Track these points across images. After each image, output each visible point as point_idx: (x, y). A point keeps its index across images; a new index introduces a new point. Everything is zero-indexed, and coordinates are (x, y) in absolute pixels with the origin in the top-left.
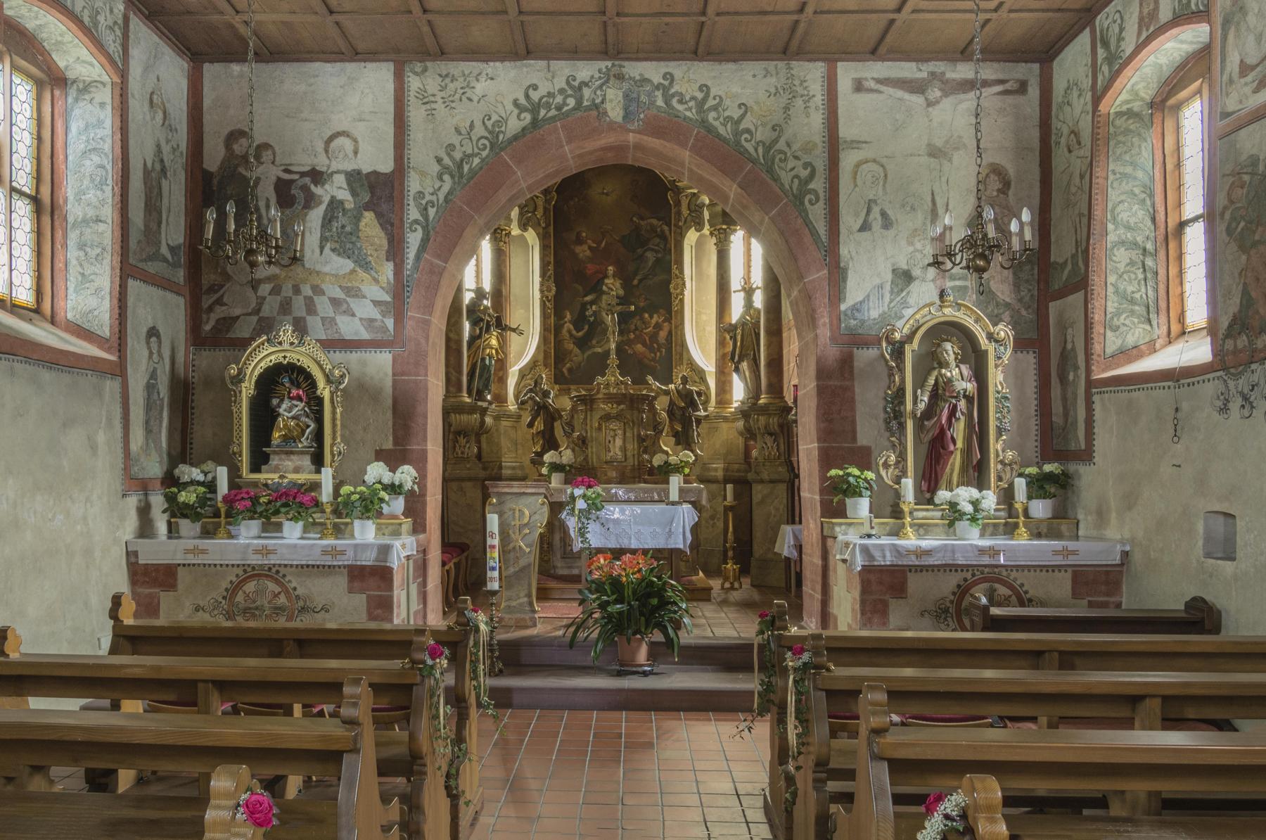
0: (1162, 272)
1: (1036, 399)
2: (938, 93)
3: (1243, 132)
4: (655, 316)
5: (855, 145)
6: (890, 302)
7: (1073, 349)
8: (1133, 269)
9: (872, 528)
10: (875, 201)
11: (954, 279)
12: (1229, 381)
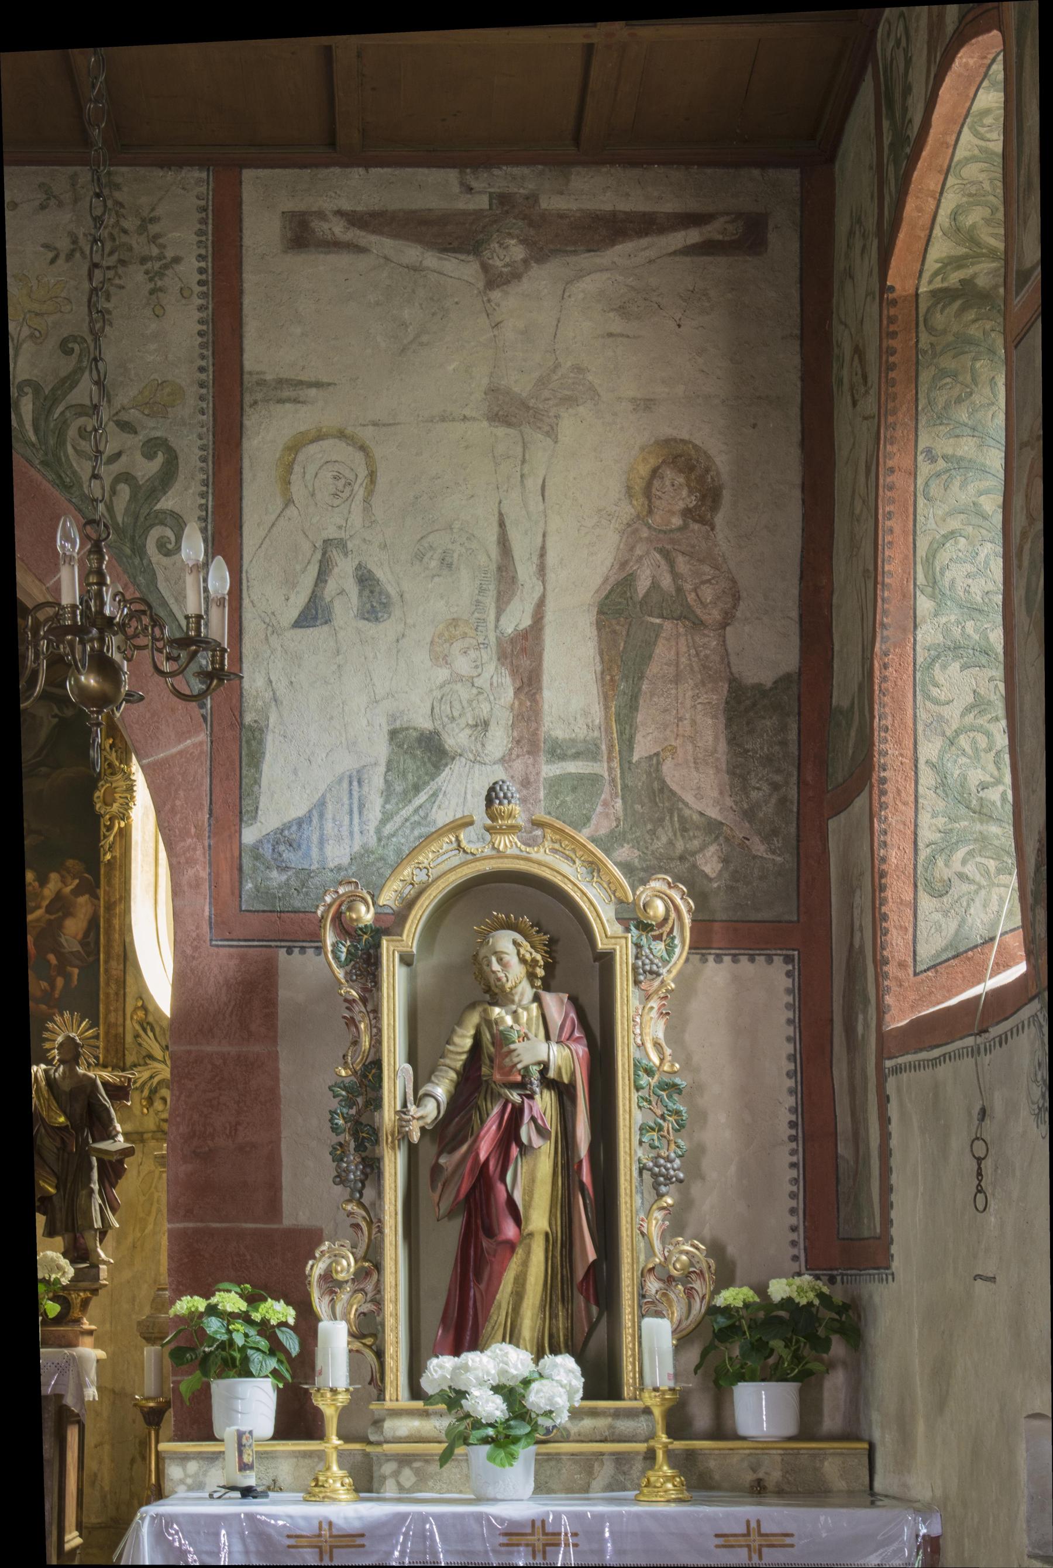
1: (792, 1092)
2: (518, 252)
4: (54, 876)
5: (286, 394)
6: (384, 822)
7: (862, 947)
8: (980, 721)
9: (244, 1467)
10: (341, 544)
11: (563, 757)
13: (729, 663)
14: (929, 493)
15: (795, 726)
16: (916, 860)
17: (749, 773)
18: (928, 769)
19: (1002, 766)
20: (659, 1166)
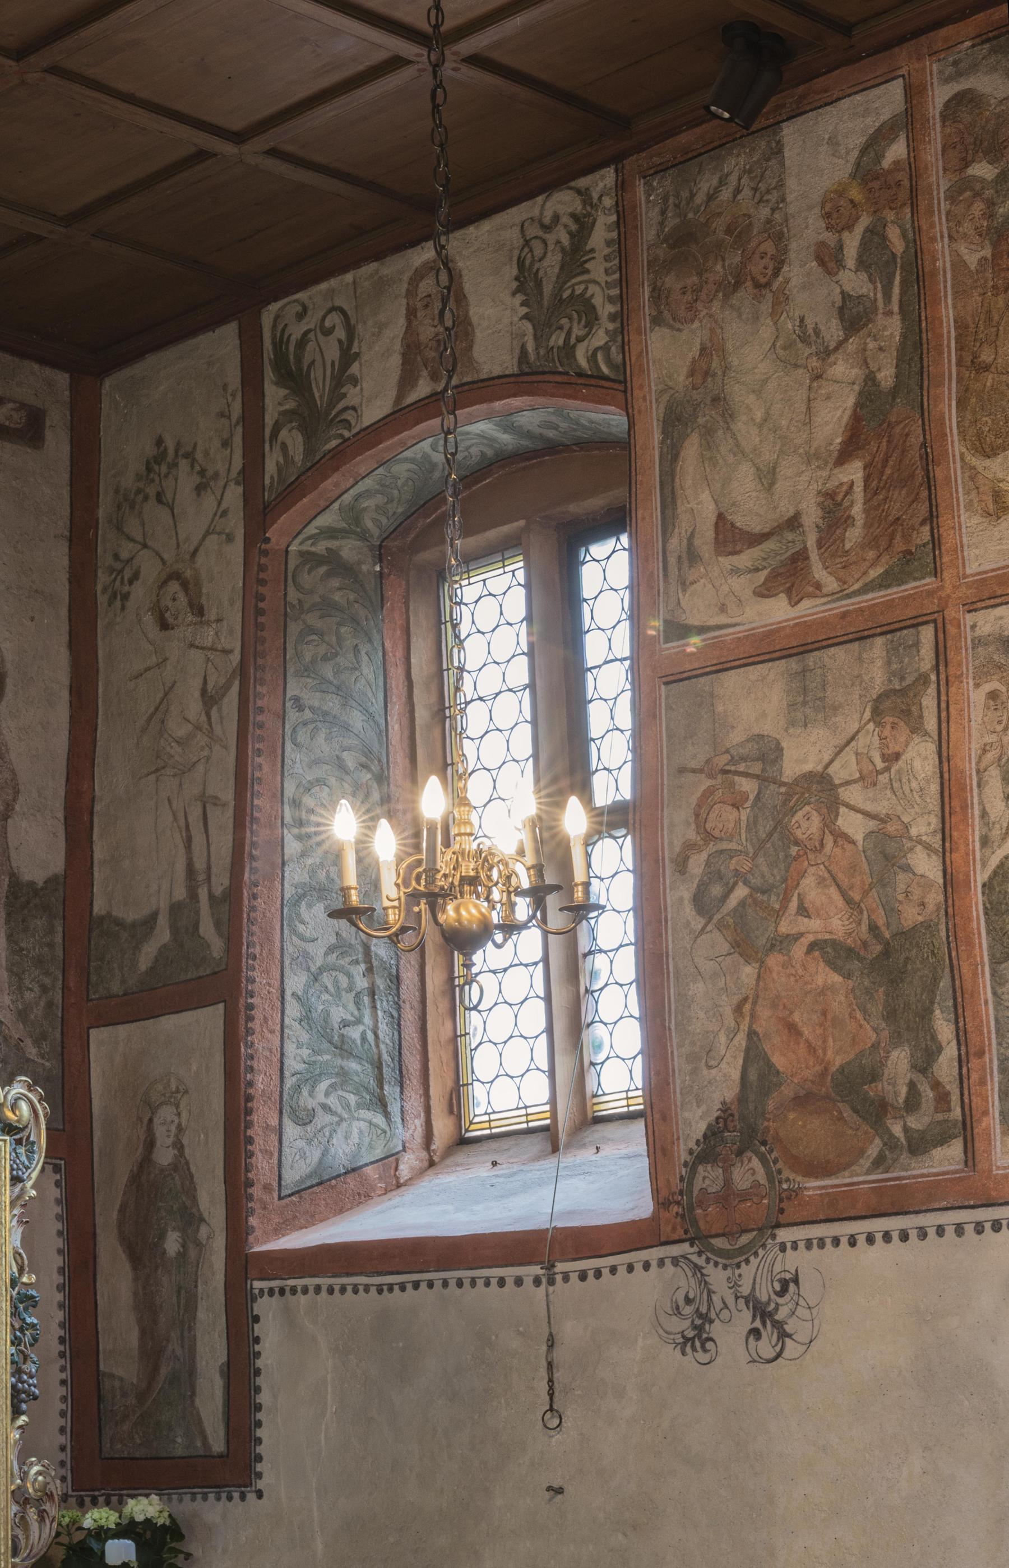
0: (409, 977)
1: (61, 1306)
3: (732, 680)
7: (181, 1165)
12: (710, 1269)
13: (9, 857)
14: (296, 739)
15: (60, 929)
16: (281, 1087)
17: (23, 972)
18: (294, 1001)
19: (361, 1007)
20: (23, 1382)
